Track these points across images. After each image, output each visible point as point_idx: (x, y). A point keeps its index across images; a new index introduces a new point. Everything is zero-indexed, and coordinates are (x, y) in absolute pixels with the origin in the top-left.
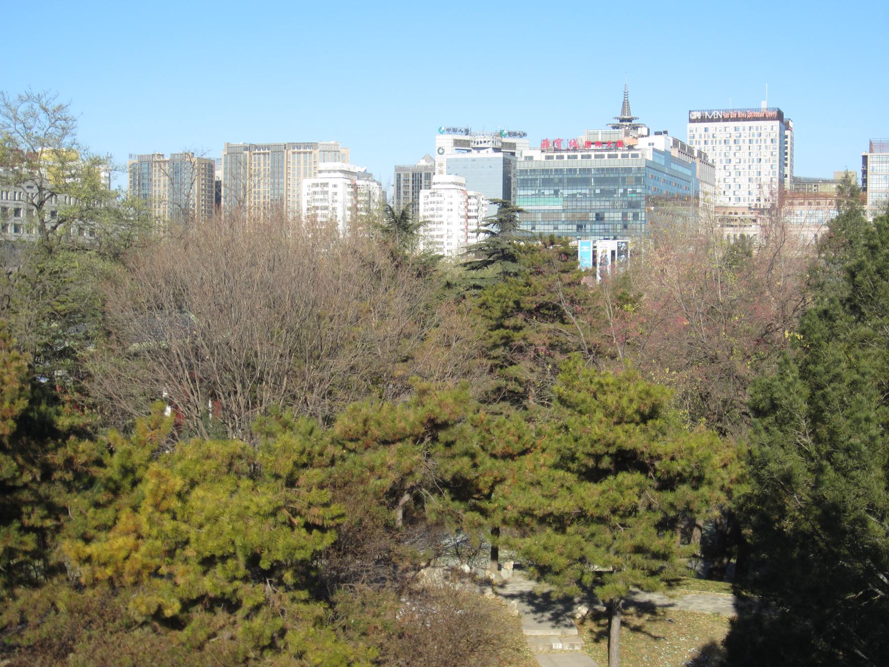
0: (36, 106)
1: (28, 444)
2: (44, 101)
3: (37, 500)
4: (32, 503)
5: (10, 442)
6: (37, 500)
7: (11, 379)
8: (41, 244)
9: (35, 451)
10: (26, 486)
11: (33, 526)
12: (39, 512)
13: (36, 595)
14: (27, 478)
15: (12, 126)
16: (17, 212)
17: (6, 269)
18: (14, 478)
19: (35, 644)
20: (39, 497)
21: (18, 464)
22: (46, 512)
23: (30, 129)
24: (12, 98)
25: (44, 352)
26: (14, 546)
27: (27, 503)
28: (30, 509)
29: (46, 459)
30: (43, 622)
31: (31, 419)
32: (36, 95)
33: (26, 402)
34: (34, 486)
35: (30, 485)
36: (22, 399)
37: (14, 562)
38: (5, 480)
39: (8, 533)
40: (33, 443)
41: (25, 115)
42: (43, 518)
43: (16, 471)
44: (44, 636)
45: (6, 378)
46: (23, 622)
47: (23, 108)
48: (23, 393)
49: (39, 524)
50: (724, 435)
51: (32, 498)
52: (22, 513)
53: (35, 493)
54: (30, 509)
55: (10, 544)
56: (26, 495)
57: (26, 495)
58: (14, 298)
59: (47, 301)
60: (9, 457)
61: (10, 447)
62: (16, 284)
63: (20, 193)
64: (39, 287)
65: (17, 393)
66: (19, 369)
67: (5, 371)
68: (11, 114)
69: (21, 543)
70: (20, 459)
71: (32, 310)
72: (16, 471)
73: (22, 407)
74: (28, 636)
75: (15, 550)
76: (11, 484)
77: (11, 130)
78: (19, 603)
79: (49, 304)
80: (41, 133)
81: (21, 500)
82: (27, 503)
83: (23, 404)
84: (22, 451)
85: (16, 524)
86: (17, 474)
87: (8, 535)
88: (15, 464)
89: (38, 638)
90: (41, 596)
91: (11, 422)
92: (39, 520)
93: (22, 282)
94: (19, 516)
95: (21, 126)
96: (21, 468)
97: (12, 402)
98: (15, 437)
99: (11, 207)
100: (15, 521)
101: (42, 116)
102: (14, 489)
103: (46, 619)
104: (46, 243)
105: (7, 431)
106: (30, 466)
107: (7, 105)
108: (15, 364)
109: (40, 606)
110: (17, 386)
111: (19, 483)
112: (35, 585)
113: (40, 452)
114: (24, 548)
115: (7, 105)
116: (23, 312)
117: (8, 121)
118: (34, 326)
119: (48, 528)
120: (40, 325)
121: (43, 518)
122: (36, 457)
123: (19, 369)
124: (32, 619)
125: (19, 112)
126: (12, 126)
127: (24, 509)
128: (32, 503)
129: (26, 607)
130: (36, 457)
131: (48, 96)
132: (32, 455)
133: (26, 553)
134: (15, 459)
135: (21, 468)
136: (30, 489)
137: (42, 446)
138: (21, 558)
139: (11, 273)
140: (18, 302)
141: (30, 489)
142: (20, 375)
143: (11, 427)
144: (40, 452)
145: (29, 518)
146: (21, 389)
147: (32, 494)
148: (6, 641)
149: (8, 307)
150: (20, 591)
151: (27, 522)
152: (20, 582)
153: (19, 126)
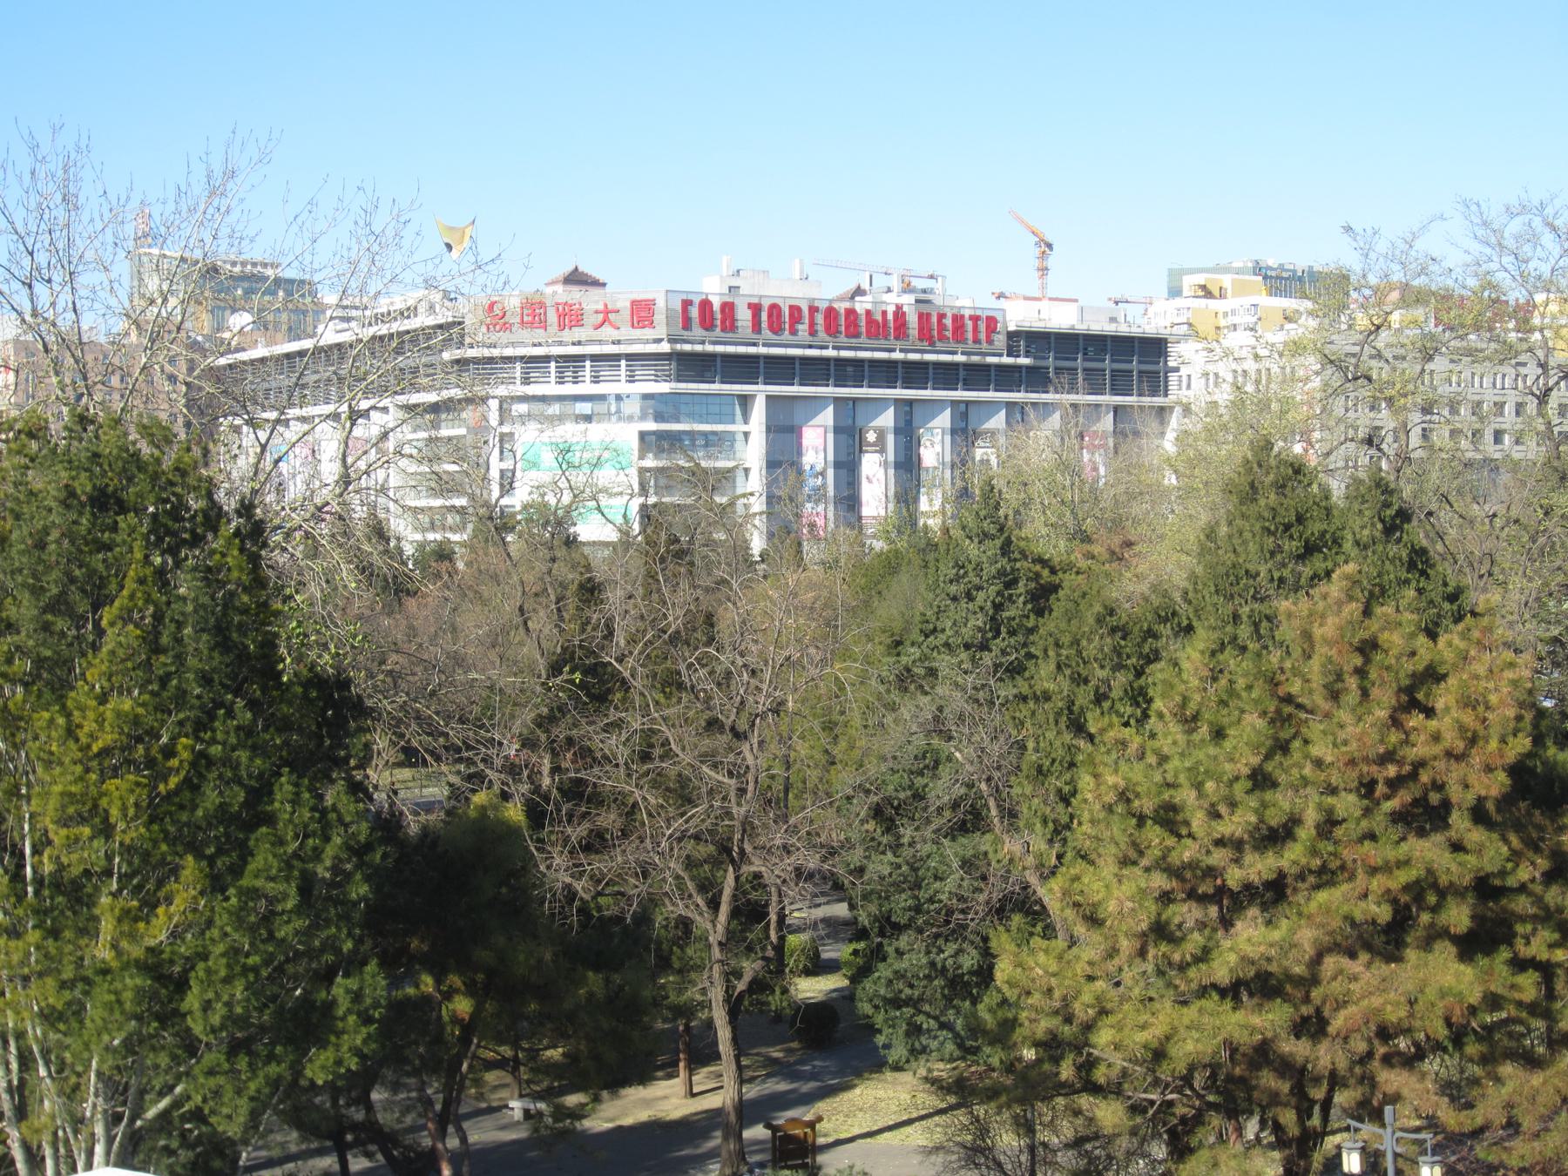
0: (1537, 222)
1: (1529, 814)
2: (1549, 211)
3: (1542, 913)
4: (1534, 918)
5: (1499, 810)
6: (1542, 913)
7: (1502, 701)
8: (1547, 463)
9: (1541, 828)
10: (1522, 888)
11: (1534, 958)
12: (1546, 935)
13: (1537, 1079)
14: (1524, 874)
15: (1495, 258)
16: (1500, 406)
17: (1487, 507)
18: (1503, 873)
19: (1532, 1166)
20: (1546, 908)
21: (1510, 849)
22: (1556, 936)
23: (1526, 262)
24: (1494, 212)
25: (1550, 653)
26: (1500, 991)
27: (1523, 919)
28: (1529, 927)
29: (1559, 843)
30: (1547, 1130)
31: (1532, 771)
32: (1536, 203)
33: (1528, 742)
34: (1538, 889)
35: (1530, 886)
36: (1520, 735)
37: (438, 1107)
38: (1488, 875)
39: (1491, 968)
40: (1537, 812)
41: (1517, 238)
42: (1551, 946)
43: (1508, 860)
44: (1549, 1154)
45: (1493, 699)
46: (1513, 1126)
47: (1515, 226)
48: (1521, 725)
49: (1544, 956)
50: (1142, 1001)
51: (1531, 911)
52: (1514, 935)
53: (1539, 900)
54: (1529, 927)
55: (1493, 988)
56: (1522, 904)
57: (1522, 904)
58: (1498, 558)
59: (1558, 563)
60: (1495, 836)
61: (1499, 819)
62: (1503, 535)
63: (1504, 376)
64: (1542, 540)
65: (1512, 725)
66: (1515, 683)
67: (1491, 685)
68: (1493, 240)
69: (1513, 986)
70: (1515, 841)
71: (1530, 580)
72: (1508, 860)
73: (1520, 749)
74: (1522, 1151)
75: (1502, 997)
76: (1497, 882)
77: (1494, 266)
78: (1506, 1091)
79: (1559, 568)
80: (1545, 270)
81: (1513, 913)
82: (1523, 919)
83: (1523, 744)
84: (1519, 827)
85: (1504, 954)
86: (1510, 865)
87: (1490, 972)
88: (1505, 849)
89: (1538, 1158)
90: (1544, 1083)
91: (1502, 777)
92: (1544, 948)
93: (1512, 530)
94: (1509, 939)
95: (1512, 258)
96: (1515, 856)
97: (1503, 741)
98: (1505, 802)
99: (1489, 398)
100: (1502, 948)
101: (1548, 238)
102: (1502, 891)
103: (1551, 1125)
104: (1556, 463)
105: (1495, 792)
106: (1530, 854)
107: (1485, 223)
108: (1509, 674)
109: (1540, 1099)
110: (1511, 713)
111: (1511, 882)
112: (1532, 1062)
113: (1550, 829)
114: (1517, 996)
115: (1485, 223)
116: (1516, 582)
117: (1488, 251)
118: (1537, 607)
119: (1559, 965)
120: (1543, 605)
121: (1551, 946)
122: (1542, 839)
123: (1515, 683)
124: (1528, 1123)
125: (1506, 235)
126: (1495, 258)
127: (1520, 928)
128: (1534, 918)
129: (1517, 1099)
130: (1542, 839)
131: (1558, 203)
132: (1534, 835)
133: (1520, 1004)
134: (1505, 840)
135: (1515, 856)
136: (1530, 894)
137: (1553, 821)
138: (1513, 1011)
139: (1494, 515)
140: (1507, 565)
141: (1530, 894)
142: (1517, 694)
143: (1503, 785)
144: (1550, 829)
145: (1528, 943)
146: (1519, 718)
147: (1533, 904)
148: (1482, 1155)
149: (1490, 575)
150: (1507, 1069)
151: (1525, 951)
152: (1510, 1055)
153: (1508, 260)
